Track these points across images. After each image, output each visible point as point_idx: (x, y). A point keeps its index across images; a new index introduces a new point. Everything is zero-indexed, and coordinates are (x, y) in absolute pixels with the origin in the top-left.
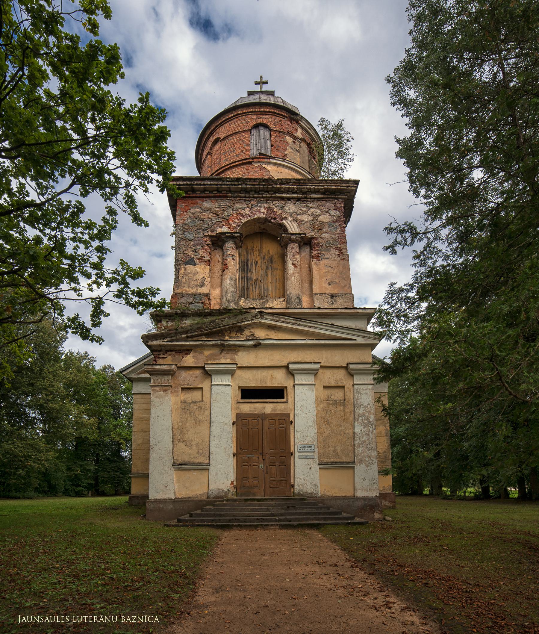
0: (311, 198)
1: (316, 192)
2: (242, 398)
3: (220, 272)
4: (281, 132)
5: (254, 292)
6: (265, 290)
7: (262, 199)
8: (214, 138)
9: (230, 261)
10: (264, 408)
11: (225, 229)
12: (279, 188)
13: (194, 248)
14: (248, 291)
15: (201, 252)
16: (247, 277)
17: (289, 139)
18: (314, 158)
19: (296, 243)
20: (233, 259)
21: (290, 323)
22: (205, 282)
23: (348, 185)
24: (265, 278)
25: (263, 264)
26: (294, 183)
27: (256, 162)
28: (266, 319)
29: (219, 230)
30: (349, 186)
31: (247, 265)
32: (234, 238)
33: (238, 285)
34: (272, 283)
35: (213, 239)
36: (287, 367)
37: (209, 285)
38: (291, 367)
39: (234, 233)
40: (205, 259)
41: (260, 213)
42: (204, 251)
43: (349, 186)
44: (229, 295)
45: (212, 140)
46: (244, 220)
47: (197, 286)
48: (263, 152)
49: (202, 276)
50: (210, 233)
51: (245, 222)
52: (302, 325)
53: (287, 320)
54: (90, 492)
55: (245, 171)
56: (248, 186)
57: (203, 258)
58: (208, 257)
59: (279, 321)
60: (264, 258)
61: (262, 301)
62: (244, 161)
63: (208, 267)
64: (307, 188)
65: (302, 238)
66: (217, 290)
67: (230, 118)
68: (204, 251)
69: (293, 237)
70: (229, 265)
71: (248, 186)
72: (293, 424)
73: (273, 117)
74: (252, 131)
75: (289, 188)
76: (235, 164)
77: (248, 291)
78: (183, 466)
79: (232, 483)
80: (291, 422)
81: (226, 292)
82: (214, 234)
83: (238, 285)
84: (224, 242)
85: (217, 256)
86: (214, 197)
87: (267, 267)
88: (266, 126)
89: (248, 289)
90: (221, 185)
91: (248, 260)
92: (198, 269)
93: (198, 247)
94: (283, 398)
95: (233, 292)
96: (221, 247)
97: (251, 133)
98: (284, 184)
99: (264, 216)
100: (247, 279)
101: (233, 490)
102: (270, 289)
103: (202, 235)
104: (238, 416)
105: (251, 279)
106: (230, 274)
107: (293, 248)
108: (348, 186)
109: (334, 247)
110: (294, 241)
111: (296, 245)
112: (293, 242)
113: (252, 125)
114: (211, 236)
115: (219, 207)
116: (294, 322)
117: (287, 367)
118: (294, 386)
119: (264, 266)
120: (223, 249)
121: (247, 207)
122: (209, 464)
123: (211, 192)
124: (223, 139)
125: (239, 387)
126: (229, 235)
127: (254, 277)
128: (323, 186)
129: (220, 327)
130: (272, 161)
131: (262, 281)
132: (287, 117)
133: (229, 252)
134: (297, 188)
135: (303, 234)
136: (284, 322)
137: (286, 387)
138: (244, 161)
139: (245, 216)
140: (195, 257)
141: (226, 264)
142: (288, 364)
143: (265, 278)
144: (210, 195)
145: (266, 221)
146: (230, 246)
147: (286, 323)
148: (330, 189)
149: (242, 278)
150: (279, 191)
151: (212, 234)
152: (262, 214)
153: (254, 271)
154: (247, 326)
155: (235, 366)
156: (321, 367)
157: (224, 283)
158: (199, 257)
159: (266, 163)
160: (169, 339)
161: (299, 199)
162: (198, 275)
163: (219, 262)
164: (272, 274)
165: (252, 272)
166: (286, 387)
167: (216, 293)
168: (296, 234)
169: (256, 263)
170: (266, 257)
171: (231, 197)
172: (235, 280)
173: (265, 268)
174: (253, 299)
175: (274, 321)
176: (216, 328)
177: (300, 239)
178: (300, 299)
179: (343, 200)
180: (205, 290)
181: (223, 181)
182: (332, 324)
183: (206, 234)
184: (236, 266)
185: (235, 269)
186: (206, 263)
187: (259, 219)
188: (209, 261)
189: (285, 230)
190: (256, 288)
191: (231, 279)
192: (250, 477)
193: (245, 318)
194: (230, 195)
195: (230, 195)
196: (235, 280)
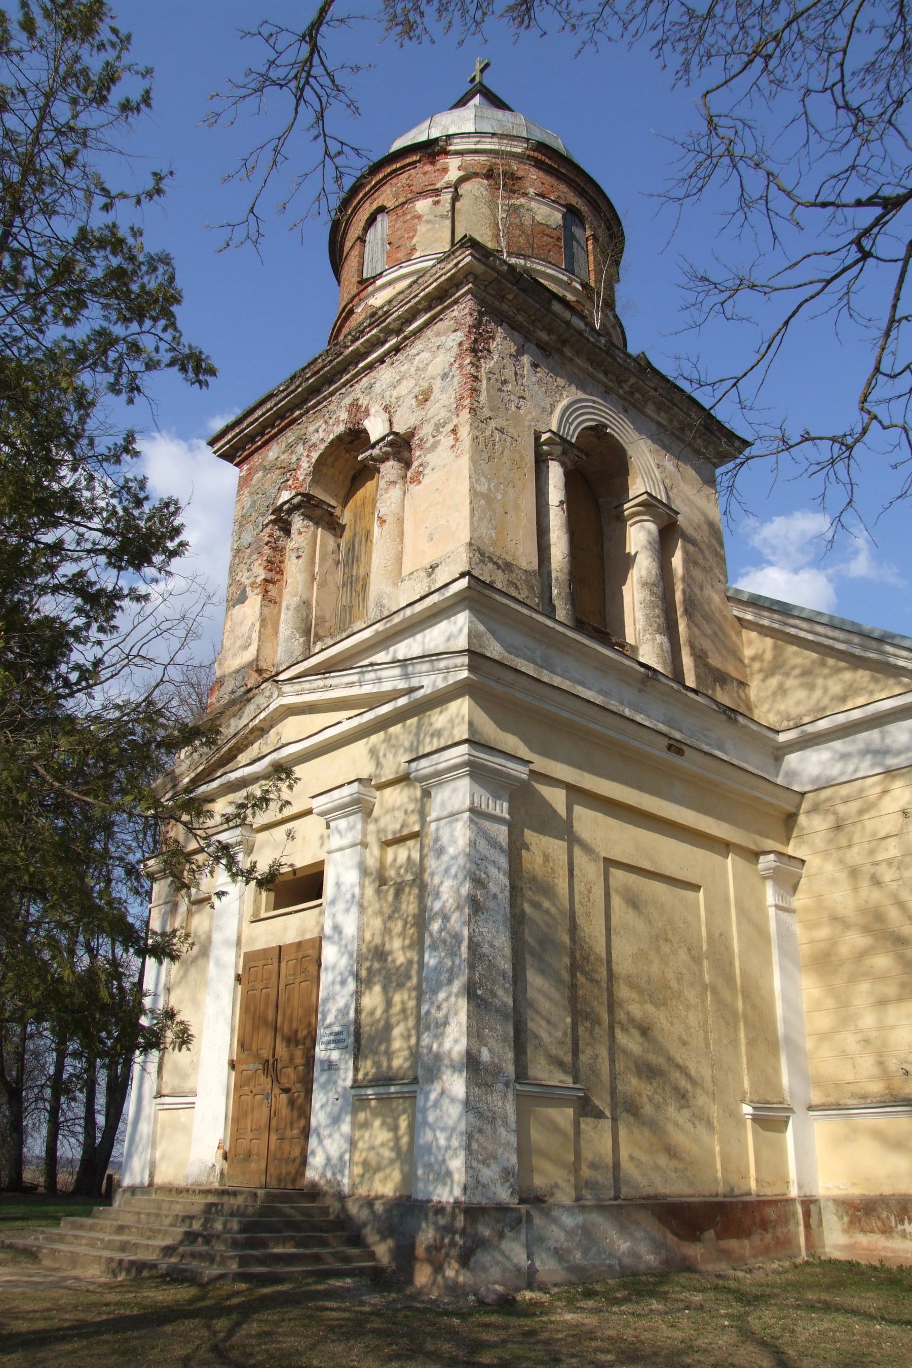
4: (405, 203)
7: (343, 390)
12: (355, 352)
19: (388, 459)
23: (455, 261)
26: (370, 325)
27: (358, 305)
30: (459, 262)
43: (459, 262)
54: (804, 1255)
64: (394, 320)
65: (390, 444)
75: (367, 340)
88: (381, 209)
98: (358, 339)
101: (220, 1164)
108: (456, 265)
110: (384, 459)
112: (383, 462)
116: (321, 683)
128: (416, 296)
129: (229, 741)
132: (419, 161)
134: (380, 331)
148: (429, 293)
150: (359, 356)
161: (397, 349)
171: (301, 415)
177: (389, 449)
179: (469, 296)
181: (276, 395)
182: (372, 665)
195: (298, 413)
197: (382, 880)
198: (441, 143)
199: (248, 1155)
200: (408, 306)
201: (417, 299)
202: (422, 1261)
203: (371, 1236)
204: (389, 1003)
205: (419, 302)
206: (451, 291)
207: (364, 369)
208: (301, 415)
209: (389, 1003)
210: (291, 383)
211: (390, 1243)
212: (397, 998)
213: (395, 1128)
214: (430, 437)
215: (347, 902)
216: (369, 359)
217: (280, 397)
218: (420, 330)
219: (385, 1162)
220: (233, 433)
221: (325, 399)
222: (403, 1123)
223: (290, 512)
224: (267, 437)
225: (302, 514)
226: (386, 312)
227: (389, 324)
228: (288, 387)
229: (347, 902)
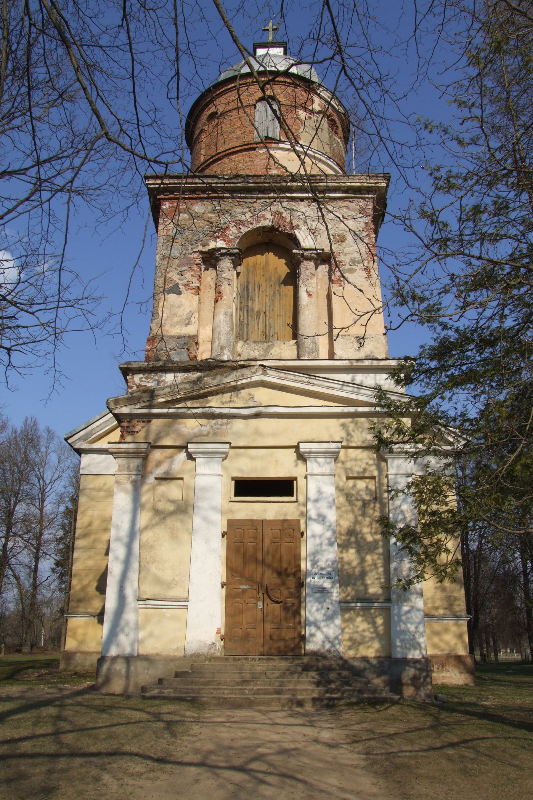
0: (330, 198)
1: (335, 190)
2: (237, 494)
3: (213, 302)
5: (257, 329)
6: (270, 327)
8: (210, 112)
9: (225, 288)
10: (265, 511)
11: (220, 244)
13: (180, 269)
14: (247, 328)
15: (188, 276)
16: (247, 306)
17: (302, 114)
18: (336, 133)
19: (310, 260)
20: (229, 285)
21: (302, 382)
22: (192, 319)
24: (271, 308)
25: (268, 288)
28: (270, 376)
29: (212, 245)
31: (248, 290)
32: (231, 255)
33: (234, 322)
34: (281, 316)
35: (205, 255)
36: (297, 448)
37: (197, 322)
38: (304, 448)
39: (232, 249)
40: (194, 285)
41: (265, 219)
42: (192, 273)
44: (222, 338)
45: (207, 113)
46: (244, 230)
47: (180, 323)
48: (270, 135)
49: (188, 310)
50: (201, 248)
51: (247, 233)
52: (317, 385)
53: (297, 378)
55: (247, 159)
56: (250, 185)
57: (191, 285)
58: (197, 282)
59: (286, 379)
60: (270, 279)
61: (266, 345)
62: (246, 147)
63: (197, 297)
65: (318, 254)
66: (207, 328)
67: (231, 88)
68: (192, 273)
69: (307, 254)
70: (223, 293)
71: (250, 185)
72: (305, 536)
73: (283, 87)
74: (257, 105)
76: (234, 150)
77: (247, 328)
78: (152, 602)
79: (218, 632)
80: (302, 534)
81: (219, 334)
82: (205, 249)
83: (234, 322)
84: (218, 260)
85: (209, 276)
86: (208, 198)
87: (274, 293)
89: (248, 325)
90: (216, 183)
91: (248, 282)
92: (184, 301)
93: (184, 268)
94: (292, 495)
95: (228, 333)
96: (215, 267)
97: (255, 108)
99: (270, 224)
100: (247, 310)
101: (220, 644)
102: (277, 325)
103: (190, 252)
104: (231, 523)
105: (252, 310)
106: (225, 307)
107: (307, 269)
108: (376, 183)
109: (361, 266)
110: (308, 259)
111: (312, 264)
113: (257, 98)
114: (201, 252)
115: (214, 211)
116: (306, 380)
117: (297, 448)
118: (306, 477)
119: (269, 291)
120: (216, 269)
121: (249, 211)
122: (187, 599)
123: (204, 192)
124: (221, 115)
125: (233, 479)
126: (225, 251)
127: (256, 308)
129: (210, 387)
130: (281, 145)
131: (267, 313)
133: (224, 275)
135: (320, 249)
136: (292, 381)
137: (296, 479)
138: (246, 147)
139: (246, 225)
140: (180, 282)
141: (220, 293)
142: (298, 443)
143: (271, 308)
144: (202, 195)
145: (272, 230)
146: (226, 264)
147: (296, 381)
148: (353, 186)
149: (241, 309)
150: (290, 190)
151: (203, 250)
152: (268, 221)
153: (256, 299)
154: (244, 387)
155: (228, 446)
156: (343, 447)
157: (217, 320)
158: (185, 282)
159: (274, 149)
160: (143, 404)
162: (183, 308)
163: (211, 288)
164: (280, 304)
165: (253, 300)
166: (296, 479)
167: (205, 334)
168: (310, 250)
169: (260, 287)
170: (273, 279)
172: (232, 315)
173: (272, 293)
174: (254, 342)
175: (280, 378)
176: (205, 388)
177: (315, 256)
178: (316, 344)
179: (372, 200)
180: (190, 330)
181: (219, 179)
183: (194, 250)
184: (233, 294)
185: (232, 299)
186: (193, 291)
187: (264, 227)
188: (198, 287)
189: (296, 242)
190: (258, 323)
191: (226, 314)
192: (244, 622)
193: (243, 375)
194: (228, 195)
195: (228, 195)
196: (232, 315)
197: (348, 497)
198: (314, 86)
199: (246, 637)
200: (337, 185)
201: (344, 185)
202: (408, 685)
203: (370, 675)
204: (363, 560)
205: (344, 186)
206: (364, 192)
207: (288, 198)
208: (228, 198)
209: (363, 560)
210: (234, 178)
211: (383, 678)
212: (369, 558)
213: (374, 623)
214: (347, 264)
215: (329, 503)
216: (295, 195)
217: (221, 181)
218: (335, 199)
219: (367, 639)
220: (171, 181)
221: (252, 198)
222: (380, 621)
223: (223, 255)
224: (195, 196)
225: (232, 260)
226: (322, 180)
227: (321, 186)
228: (231, 179)
229: (329, 503)
